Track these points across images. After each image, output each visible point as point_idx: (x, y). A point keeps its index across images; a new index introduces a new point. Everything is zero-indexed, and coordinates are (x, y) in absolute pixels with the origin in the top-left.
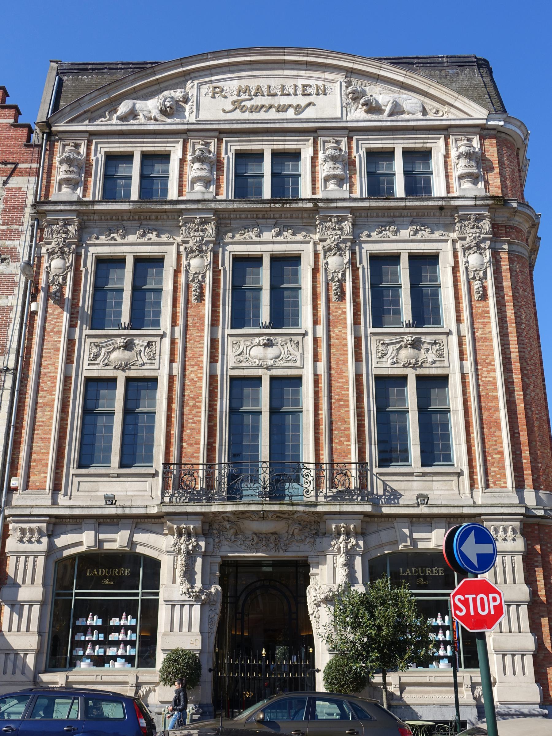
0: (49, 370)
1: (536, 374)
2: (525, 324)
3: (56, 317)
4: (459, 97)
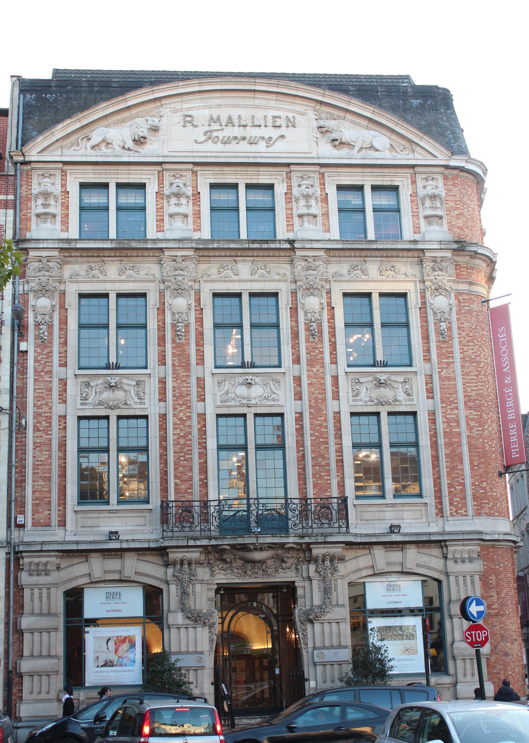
0: (43, 411)
1: (493, 410)
2: (483, 362)
3: (45, 356)
4: (424, 137)
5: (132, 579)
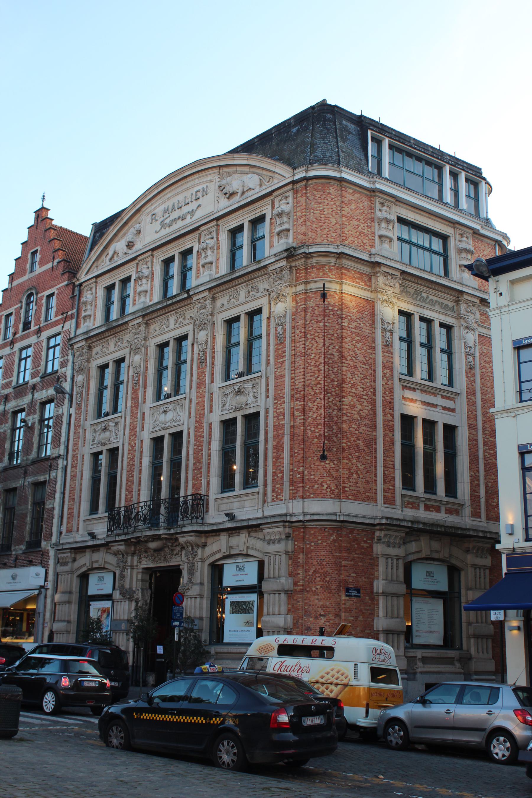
2: (315, 353)
5: (102, 566)
